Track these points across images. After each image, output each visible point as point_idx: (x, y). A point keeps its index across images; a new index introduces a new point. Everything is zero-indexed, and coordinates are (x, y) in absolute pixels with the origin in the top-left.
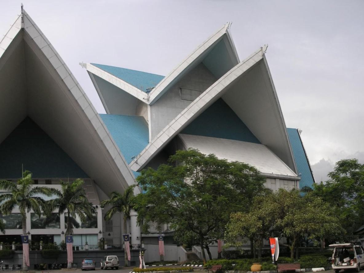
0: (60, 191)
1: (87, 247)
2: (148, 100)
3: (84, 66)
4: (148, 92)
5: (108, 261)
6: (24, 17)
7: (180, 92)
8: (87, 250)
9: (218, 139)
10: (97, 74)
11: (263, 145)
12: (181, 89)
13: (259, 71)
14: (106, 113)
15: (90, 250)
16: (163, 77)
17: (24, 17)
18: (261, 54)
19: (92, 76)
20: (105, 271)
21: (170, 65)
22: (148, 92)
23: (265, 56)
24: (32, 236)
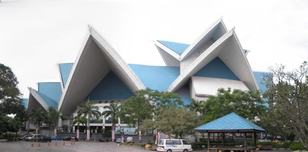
0: (207, 100)
1: (127, 133)
2: (180, 59)
3: (153, 41)
4: (180, 55)
5: (164, 139)
6: (91, 29)
7: (198, 54)
8: (128, 134)
9: (213, 78)
10: (160, 47)
11: (242, 82)
12: (199, 52)
13: (232, 40)
14: (37, 90)
15: (129, 134)
16: (190, 45)
17: (91, 29)
18: (232, 32)
19: (158, 47)
20: (89, 143)
21: (193, 39)
22: (180, 55)
23: (235, 32)
24: (106, 127)
